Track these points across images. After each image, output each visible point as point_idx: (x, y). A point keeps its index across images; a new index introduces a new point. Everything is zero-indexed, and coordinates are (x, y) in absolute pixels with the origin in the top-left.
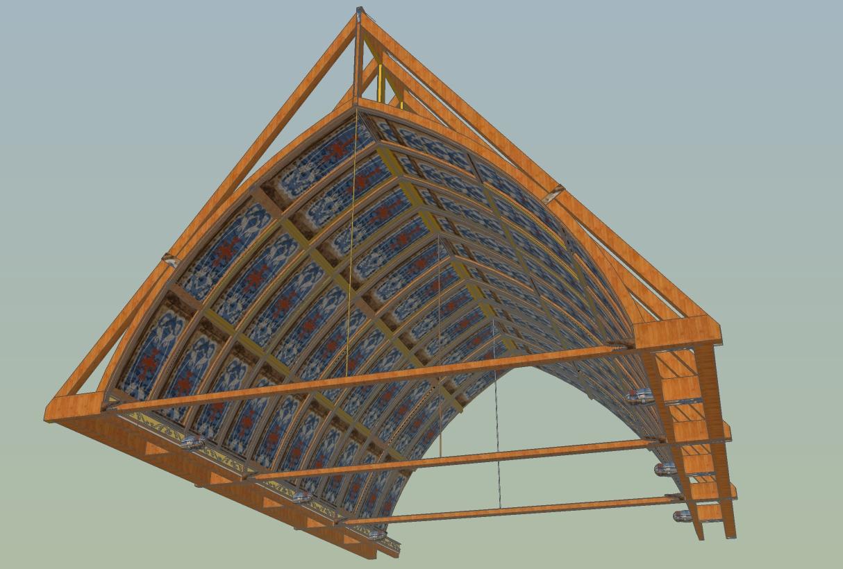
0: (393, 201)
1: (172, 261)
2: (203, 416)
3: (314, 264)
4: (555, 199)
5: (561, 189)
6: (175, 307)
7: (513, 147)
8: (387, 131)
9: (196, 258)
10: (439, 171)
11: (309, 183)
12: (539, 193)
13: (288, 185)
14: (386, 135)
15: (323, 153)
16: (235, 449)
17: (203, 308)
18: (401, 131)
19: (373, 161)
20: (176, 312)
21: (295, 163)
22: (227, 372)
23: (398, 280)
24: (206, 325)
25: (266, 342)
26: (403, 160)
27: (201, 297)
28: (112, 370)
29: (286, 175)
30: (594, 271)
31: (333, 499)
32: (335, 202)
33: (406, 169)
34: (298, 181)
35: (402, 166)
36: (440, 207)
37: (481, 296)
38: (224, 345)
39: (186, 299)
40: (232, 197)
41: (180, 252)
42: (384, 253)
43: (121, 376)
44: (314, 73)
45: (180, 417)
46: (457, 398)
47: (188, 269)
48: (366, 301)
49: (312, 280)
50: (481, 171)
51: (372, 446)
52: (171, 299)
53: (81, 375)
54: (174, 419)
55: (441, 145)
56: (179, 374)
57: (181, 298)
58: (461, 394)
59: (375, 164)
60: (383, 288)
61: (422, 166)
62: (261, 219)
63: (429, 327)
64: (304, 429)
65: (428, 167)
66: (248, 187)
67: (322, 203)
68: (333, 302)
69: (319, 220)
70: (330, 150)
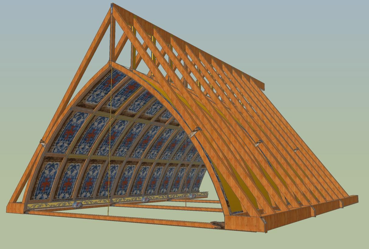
44: (20, 184)
45: (69, 196)
53: (64, 103)
54: (66, 198)
56: (63, 181)
70: (87, 186)
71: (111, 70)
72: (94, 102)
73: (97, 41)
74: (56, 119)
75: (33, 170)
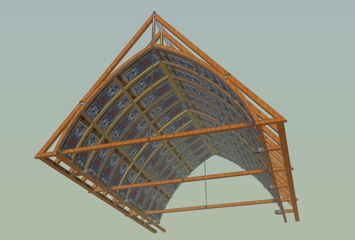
0: (173, 97)
1: (83, 103)
2: (79, 157)
3: (135, 109)
4: (227, 78)
5: (229, 74)
6: (95, 133)
7: (211, 60)
8: (164, 57)
9: (92, 103)
10: (191, 86)
11: (135, 76)
12: (221, 76)
13: (127, 77)
14: (191, 108)
15: (140, 65)
16: (103, 181)
17: (105, 134)
18: (177, 71)
19: (166, 83)
20: (95, 135)
21: (129, 68)
22: (112, 159)
23: (167, 118)
24: (94, 130)
25: (116, 139)
26: (184, 94)
27: (93, 118)
28: (60, 144)
29: (126, 72)
30: (242, 105)
31: (140, 207)
32: (144, 85)
33: (171, 72)
34: (130, 75)
35: (169, 72)
36: (201, 120)
37: (211, 147)
38: (101, 139)
39: (87, 119)
40: (106, 80)
41: (86, 100)
42: (154, 96)
43: (76, 157)
46: (188, 168)
47: (89, 107)
48: (154, 126)
49: (115, 91)
50: (200, 70)
51: (142, 175)
52: (82, 118)
53: (47, 146)
55: (191, 75)
57: (86, 118)
58: (190, 167)
59: (174, 96)
60: (161, 121)
61: (177, 71)
62: (116, 89)
63: (193, 158)
64: (130, 177)
65: (179, 71)
66: (112, 76)
67: (139, 85)
68: (142, 126)
69: (138, 92)
71: (152, 50)
72: (127, 79)
73: (140, 33)
74: (97, 85)
75: (69, 124)
